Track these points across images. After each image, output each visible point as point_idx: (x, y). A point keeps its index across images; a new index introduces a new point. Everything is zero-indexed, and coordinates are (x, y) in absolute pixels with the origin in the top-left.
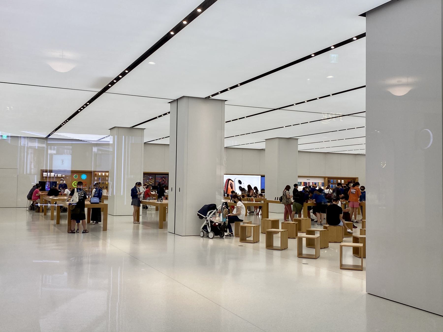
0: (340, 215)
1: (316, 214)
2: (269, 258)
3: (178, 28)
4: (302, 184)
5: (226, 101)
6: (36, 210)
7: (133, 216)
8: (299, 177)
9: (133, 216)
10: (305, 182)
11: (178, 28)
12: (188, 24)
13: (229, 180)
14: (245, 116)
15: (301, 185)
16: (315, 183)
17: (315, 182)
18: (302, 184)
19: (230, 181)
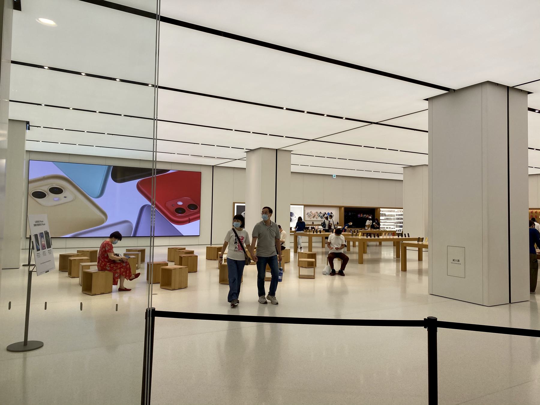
5: (529, 93)
7: (423, 251)
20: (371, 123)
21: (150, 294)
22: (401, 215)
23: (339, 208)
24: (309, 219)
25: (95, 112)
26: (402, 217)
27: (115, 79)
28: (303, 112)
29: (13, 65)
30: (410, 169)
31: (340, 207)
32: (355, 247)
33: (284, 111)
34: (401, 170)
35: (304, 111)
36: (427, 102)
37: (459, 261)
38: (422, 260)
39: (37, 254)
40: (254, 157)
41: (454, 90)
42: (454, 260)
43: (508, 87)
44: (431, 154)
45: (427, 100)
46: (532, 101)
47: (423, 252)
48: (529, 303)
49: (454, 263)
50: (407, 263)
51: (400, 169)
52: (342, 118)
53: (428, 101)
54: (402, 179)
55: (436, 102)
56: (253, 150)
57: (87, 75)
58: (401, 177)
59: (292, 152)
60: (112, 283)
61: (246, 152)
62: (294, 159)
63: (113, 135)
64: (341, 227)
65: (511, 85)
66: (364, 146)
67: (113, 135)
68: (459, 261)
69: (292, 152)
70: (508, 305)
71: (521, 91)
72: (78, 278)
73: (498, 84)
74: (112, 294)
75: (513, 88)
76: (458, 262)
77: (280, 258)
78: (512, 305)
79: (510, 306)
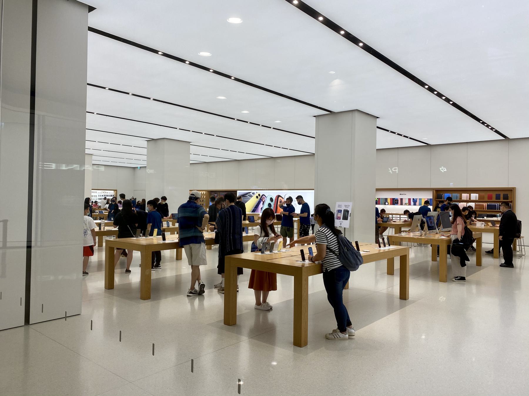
0: (260, 253)
1: (259, 245)
2: (470, 282)
3: (448, 100)
4: (389, 201)
5: (378, 118)
6: (304, 232)
7: (493, 244)
8: (378, 190)
9: (493, 244)
10: (393, 199)
11: (448, 100)
12: (295, 6)
13: (279, 196)
14: (234, 75)
15: (387, 203)
16: (413, 199)
17: (415, 198)
18: (389, 201)
19: (280, 198)
21: (377, 282)
25: (190, 131)
27: (234, 119)
28: (247, 122)
33: (271, 129)
34: (145, 144)
35: (132, 95)
39: (326, 252)
45: (315, 116)
47: (482, 243)
50: (169, 250)
57: (238, 120)
59: (191, 144)
63: (116, 133)
66: (274, 146)
67: (116, 133)
69: (191, 144)
70: (23, 328)
74: (395, 279)
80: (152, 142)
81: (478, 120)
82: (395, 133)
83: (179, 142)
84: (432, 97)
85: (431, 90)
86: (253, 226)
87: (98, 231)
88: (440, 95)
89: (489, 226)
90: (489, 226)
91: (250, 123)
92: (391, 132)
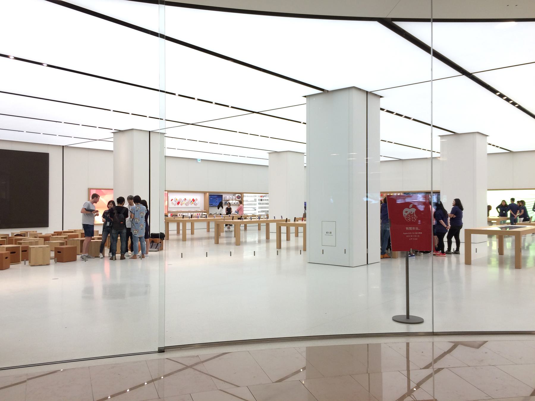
5: (488, 136)
7: (464, 243)
9: (464, 243)
11: (514, 104)
20: (253, 112)
22: (267, 200)
23: (203, 194)
24: (173, 206)
26: (268, 202)
29: (306, 143)
30: (276, 154)
31: (205, 193)
32: (186, 241)
34: (267, 156)
36: (305, 98)
37: (331, 233)
38: (290, 240)
40: (123, 138)
41: (328, 91)
42: (327, 233)
43: (367, 92)
44: (308, 143)
45: (305, 97)
46: (383, 103)
48: (379, 264)
49: (327, 235)
51: (266, 155)
52: (228, 106)
53: (306, 98)
54: (113, 150)
55: (314, 99)
56: (122, 131)
58: (266, 163)
60: (99, 251)
61: (113, 133)
62: (168, 142)
64: (122, 223)
65: (369, 90)
66: (250, 134)
68: (331, 233)
71: (376, 95)
72: (210, 222)
73: (360, 89)
75: (371, 93)
76: (331, 234)
77: (152, 244)
78: (369, 265)
79: (367, 267)
80: (274, 155)
81: (494, 91)
82: (397, 114)
83: (141, 132)
84: (502, 101)
85: (501, 96)
86: (94, 231)
87: (498, 218)
88: (508, 100)
89: (224, 233)
90: (224, 233)
91: (216, 104)
92: (406, 117)
